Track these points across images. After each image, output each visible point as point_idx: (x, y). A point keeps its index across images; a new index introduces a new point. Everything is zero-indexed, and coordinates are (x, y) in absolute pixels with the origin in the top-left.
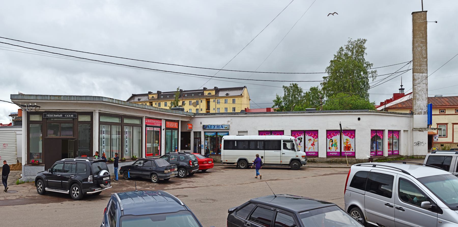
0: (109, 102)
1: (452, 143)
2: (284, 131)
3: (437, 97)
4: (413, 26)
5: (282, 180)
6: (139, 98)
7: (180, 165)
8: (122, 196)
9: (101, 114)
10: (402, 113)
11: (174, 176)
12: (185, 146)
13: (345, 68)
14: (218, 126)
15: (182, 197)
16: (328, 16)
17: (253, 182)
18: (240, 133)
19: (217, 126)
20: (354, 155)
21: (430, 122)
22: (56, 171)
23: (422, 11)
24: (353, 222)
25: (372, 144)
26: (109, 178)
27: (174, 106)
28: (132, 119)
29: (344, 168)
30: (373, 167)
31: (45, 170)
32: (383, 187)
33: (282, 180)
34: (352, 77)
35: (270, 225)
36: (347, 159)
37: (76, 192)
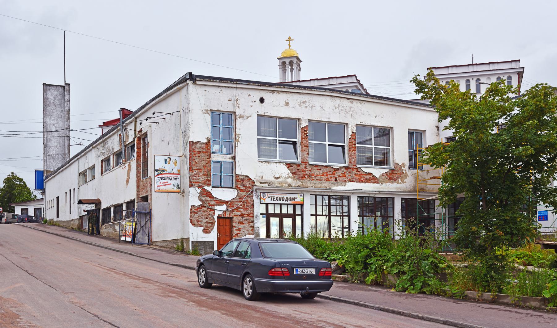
25: (469, 299)
28: (18, 205)
29: (283, 141)
36: (278, 139)
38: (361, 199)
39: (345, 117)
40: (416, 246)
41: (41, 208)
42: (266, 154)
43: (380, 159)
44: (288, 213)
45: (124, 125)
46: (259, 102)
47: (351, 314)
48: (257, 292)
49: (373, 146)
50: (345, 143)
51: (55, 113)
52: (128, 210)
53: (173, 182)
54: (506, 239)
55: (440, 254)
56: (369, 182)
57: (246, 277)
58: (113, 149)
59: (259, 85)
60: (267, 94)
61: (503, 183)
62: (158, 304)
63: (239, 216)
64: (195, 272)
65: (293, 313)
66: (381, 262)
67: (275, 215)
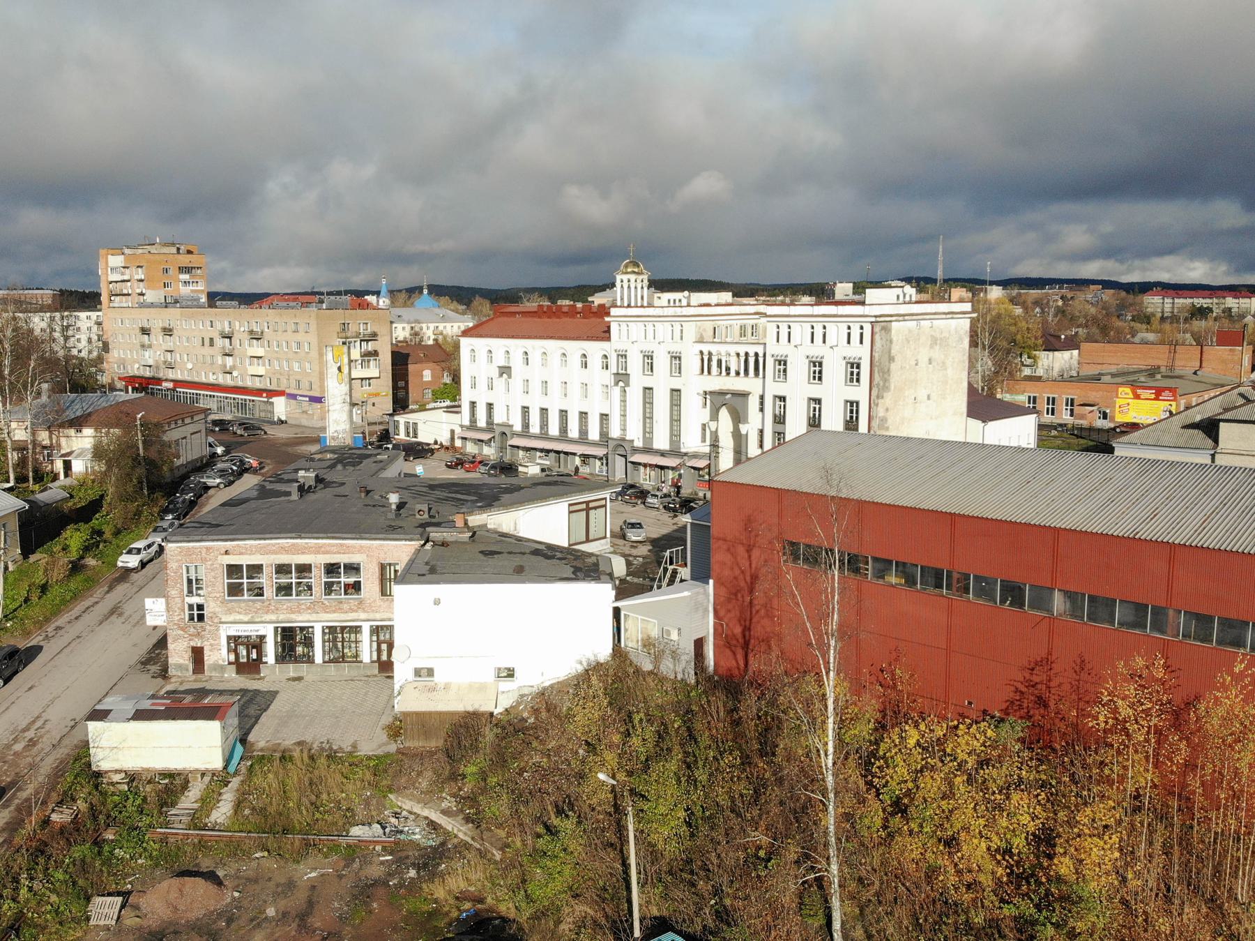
2: (603, 339)
3: (1077, 429)
4: (597, 488)
5: (339, 293)
6: (244, 560)
7: (1084, 227)
8: (1122, 384)
10: (1104, 259)
11: (605, 468)
12: (243, 663)
13: (284, 868)
14: (724, 373)
15: (1169, 578)
16: (812, 342)
17: (293, 683)
18: (1234, 351)
19: (728, 374)
20: (571, 515)
21: (70, 613)
22: (779, 423)
24: (329, 456)
26: (386, 645)
27: (103, 469)
28: (444, 482)
30: (775, 416)
31: (457, 347)
32: (534, 306)
33: (339, 293)
34: (1063, 762)
35: (887, 429)
36: (245, 581)
37: (1118, 430)
38: (1190, 637)
39: (566, 383)
40: (1009, 830)
41: (744, 395)
43: (506, 909)
44: (985, 443)
45: (515, 872)
46: (695, 638)
47: (449, 736)
48: (1032, 446)
49: (245, 581)
50: (356, 630)
52: (1073, 611)
53: (160, 618)
54: (73, 764)
55: (381, 859)
56: (974, 343)
57: (431, 364)
58: (1114, 294)
59: (188, 699)
60: (1170, 280)
61: (586, 741)
62: (1101, 902)
63: (493, 467)
64: (616, 372)
65: (273, 557)
66: (930, 749)
67: (384, 642)
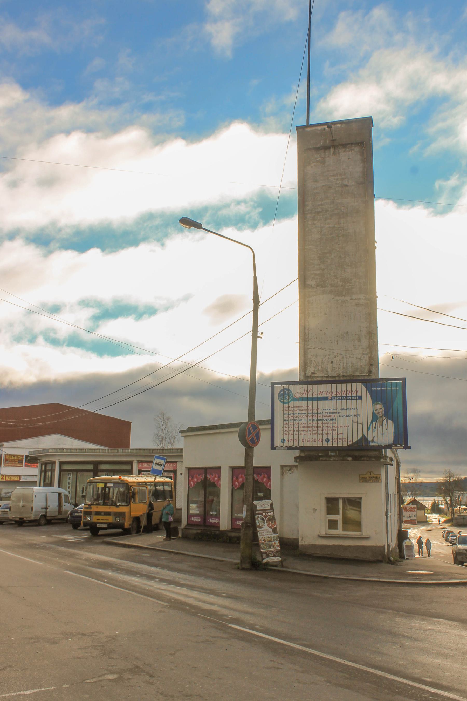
0: (58, 452)
1: (308, 125)
9: (62, 463)
23: (305, 124)
42: (327, 404)
51: (339, 281)
